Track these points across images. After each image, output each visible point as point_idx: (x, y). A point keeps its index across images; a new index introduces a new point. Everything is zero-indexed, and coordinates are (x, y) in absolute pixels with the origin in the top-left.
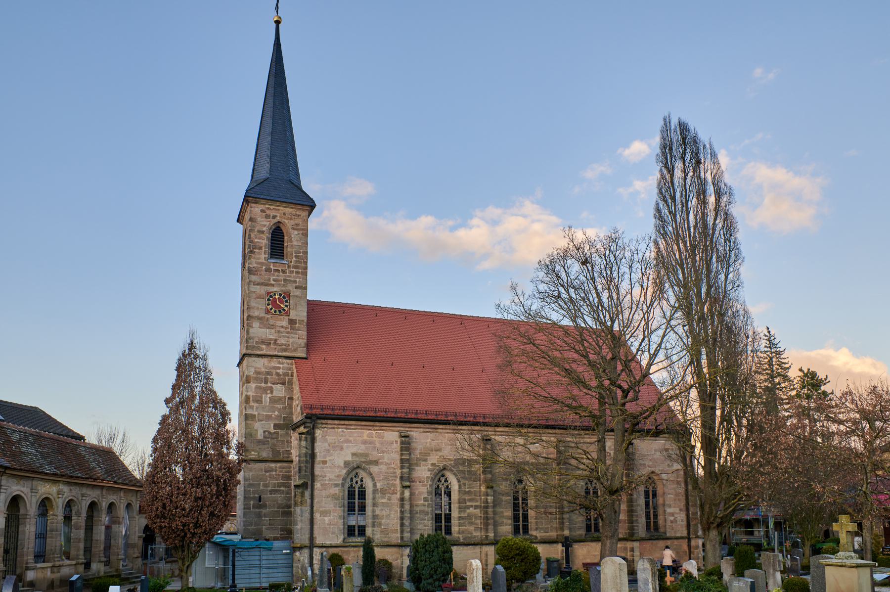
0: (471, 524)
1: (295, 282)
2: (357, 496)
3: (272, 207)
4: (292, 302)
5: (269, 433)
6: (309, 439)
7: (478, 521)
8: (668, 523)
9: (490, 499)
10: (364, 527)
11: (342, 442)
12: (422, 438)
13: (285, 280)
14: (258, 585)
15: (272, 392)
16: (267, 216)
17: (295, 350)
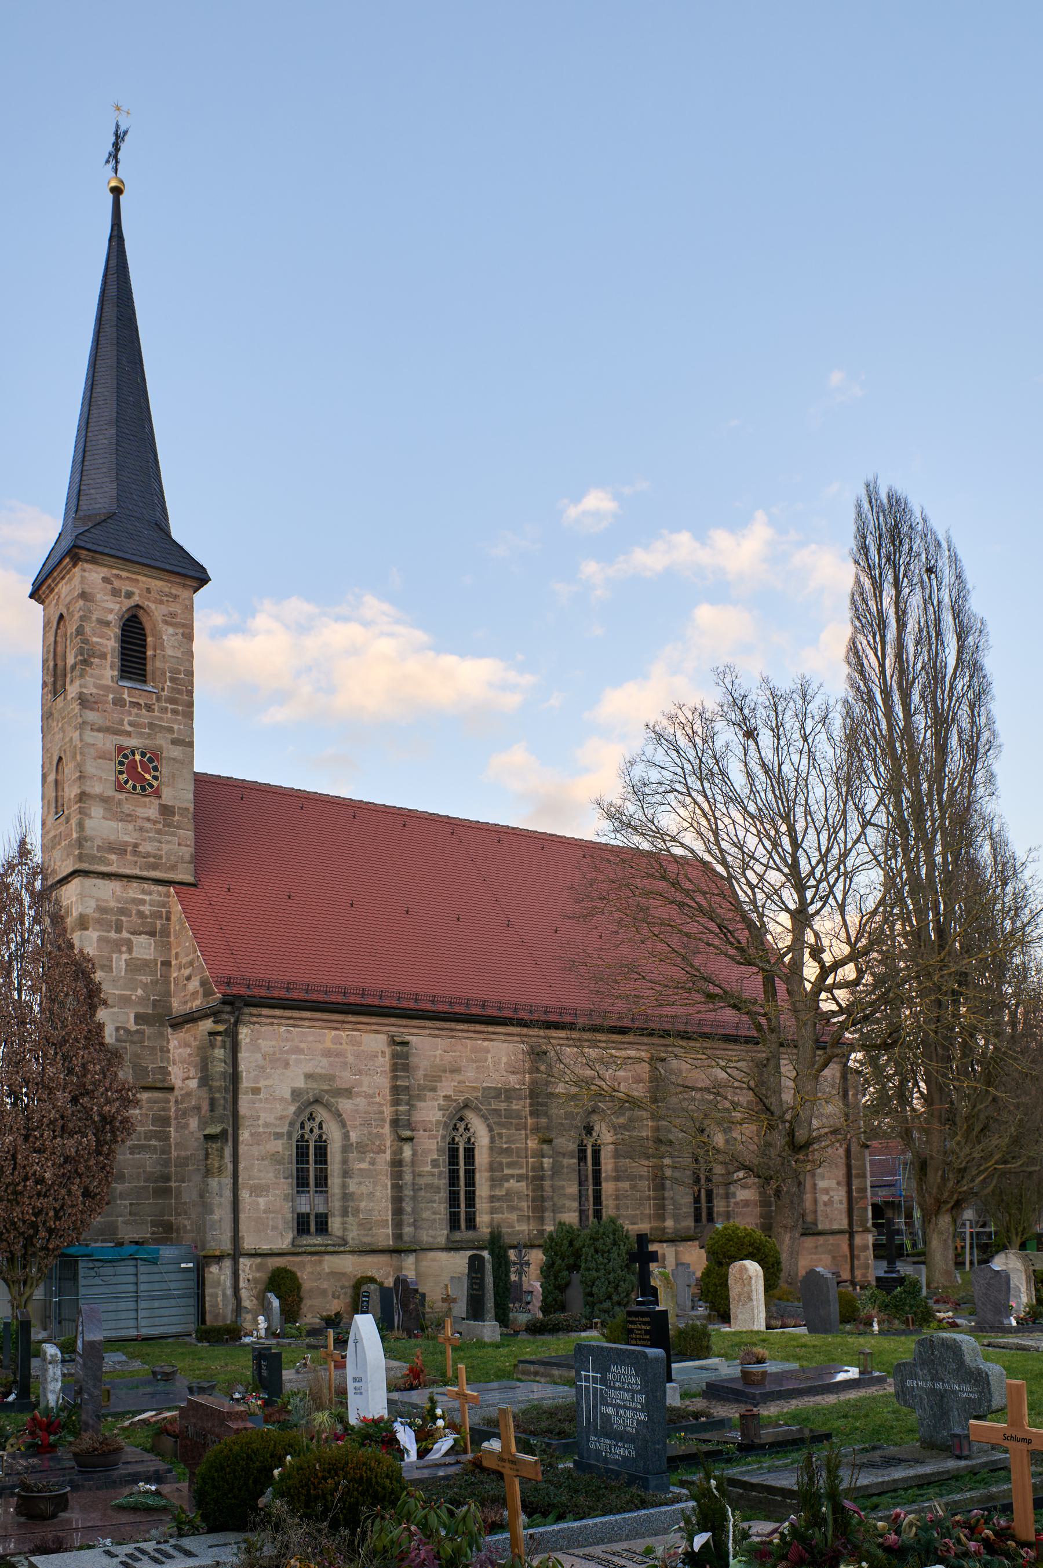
0: (512, 1209)
1: (171, 730)
2: (312, 1158)
3: (124, 574)
4: (165, 770)
5: (127, 1031)
6: (228, 1045)
7: (524, 1205)
8: (821, 1207)
9: (547, 1162)
10: (326, 1216)
11: (287, 1052)
12: (430, 1047)
13: (151, 725)
14: (133, 1333)
15: (130, 950)
16: (116, 593)
17: (173, 868)
